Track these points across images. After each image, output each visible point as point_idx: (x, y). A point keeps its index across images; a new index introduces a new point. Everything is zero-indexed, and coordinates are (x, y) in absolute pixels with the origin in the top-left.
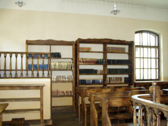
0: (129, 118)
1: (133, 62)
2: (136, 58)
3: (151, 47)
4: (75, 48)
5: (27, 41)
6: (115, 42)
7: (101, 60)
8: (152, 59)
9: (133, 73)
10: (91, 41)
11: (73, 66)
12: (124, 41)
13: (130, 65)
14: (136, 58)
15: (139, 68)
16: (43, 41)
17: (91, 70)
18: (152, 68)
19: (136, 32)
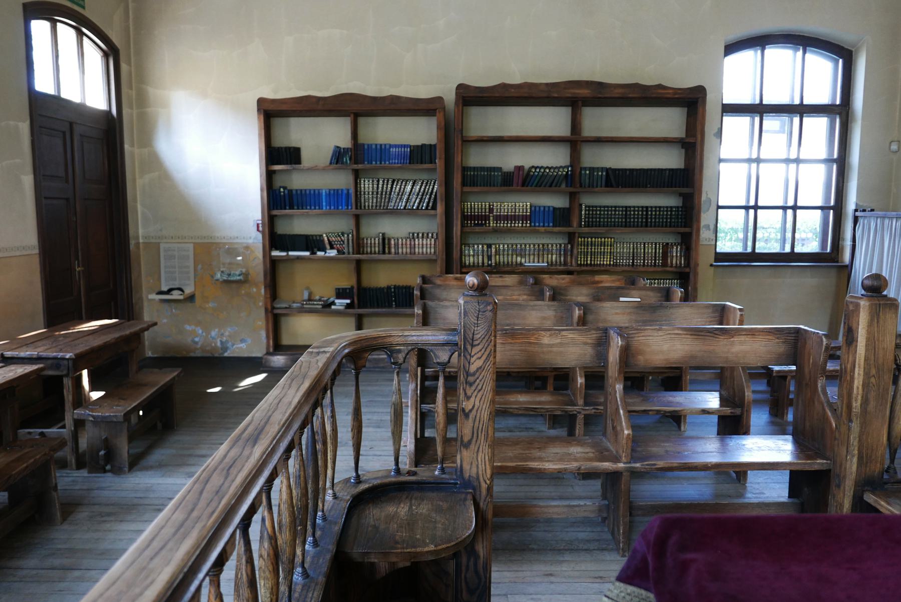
0: (559, 413)
1: (697, 176)
2: (721, 161)
3: (802, 110)
4: (322, 369)
5: (261, 102)
6: (617, 93)
7: (510, 172)
8: (761, 165)
9: (695, 227)
10: (513, 93)
11: (207, 470)
12: (660, 86)
13: (685, 190)
14: (721, 161)
15: (759, 211)
16: (319, 99)
17: (283, 149)
18: (799, 211)
19: (731, 48)
